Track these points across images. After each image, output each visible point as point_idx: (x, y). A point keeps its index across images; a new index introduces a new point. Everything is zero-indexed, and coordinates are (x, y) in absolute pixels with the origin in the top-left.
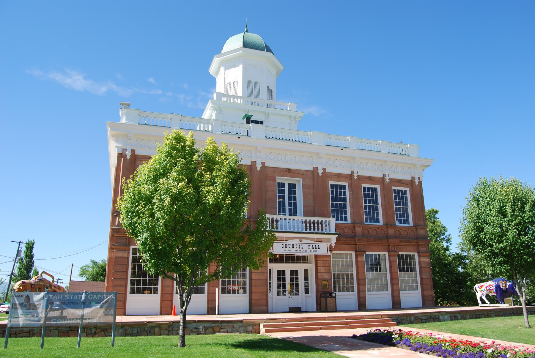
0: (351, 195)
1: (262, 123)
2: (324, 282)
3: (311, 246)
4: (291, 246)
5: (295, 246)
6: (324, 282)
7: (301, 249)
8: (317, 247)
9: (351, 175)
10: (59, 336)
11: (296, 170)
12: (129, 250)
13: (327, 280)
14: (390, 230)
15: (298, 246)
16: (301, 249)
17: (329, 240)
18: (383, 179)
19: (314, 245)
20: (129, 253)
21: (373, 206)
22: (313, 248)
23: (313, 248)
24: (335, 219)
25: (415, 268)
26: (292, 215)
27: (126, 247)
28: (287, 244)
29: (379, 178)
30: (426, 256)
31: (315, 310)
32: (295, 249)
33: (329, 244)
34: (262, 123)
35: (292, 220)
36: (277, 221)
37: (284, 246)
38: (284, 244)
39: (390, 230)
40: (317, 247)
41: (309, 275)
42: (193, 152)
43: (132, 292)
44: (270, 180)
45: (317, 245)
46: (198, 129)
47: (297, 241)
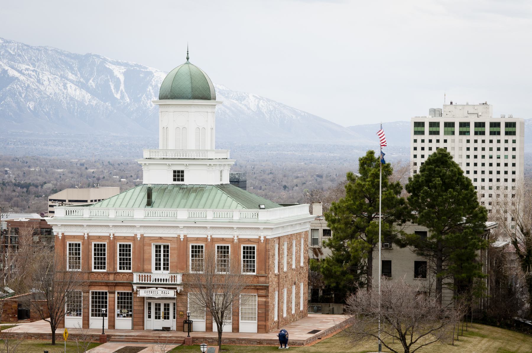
2: (181, 313)
17: (176, 288)
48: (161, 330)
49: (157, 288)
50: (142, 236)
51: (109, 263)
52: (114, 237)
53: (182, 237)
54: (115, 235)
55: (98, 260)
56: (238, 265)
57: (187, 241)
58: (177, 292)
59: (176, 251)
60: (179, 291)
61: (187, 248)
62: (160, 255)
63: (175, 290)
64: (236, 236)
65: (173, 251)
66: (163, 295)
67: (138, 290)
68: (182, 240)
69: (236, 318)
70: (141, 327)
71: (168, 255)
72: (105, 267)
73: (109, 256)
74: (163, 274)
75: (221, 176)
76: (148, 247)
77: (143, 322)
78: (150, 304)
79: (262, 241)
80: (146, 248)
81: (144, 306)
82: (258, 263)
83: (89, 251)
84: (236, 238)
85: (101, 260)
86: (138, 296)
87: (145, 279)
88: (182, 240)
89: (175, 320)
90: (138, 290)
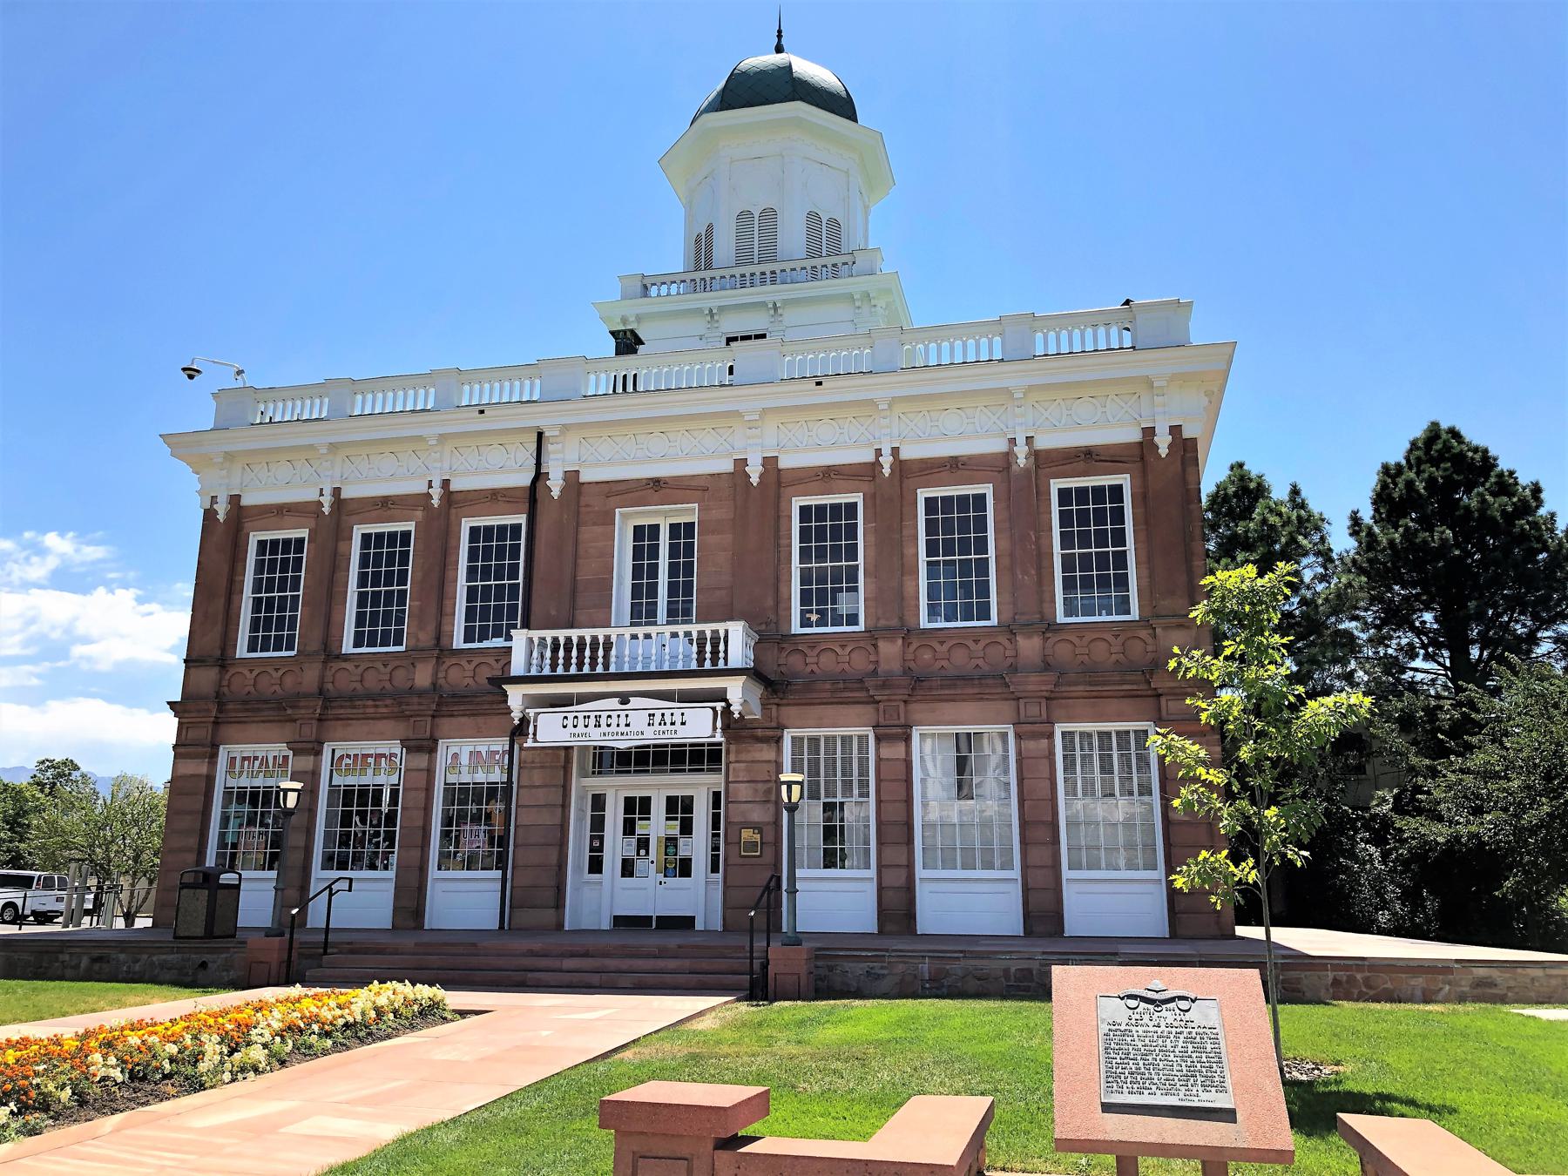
0: (1044, 557)
1: (763, 336)
2: (747, 834)
4: (592, 721)
5: (603, 721)
6: (747, 834)
7: (623, 728)
9: (873, 464)
11: (970, 457)
12: (1051, 736)
13: (757, 827)
14: (1022, 642)
16: (623, 728)
18: (1008, 457)
19: (667, 713)
20: (779, 751)
21: (487, 589)
22: (663, 722)
23: (663, 722)
24: (513, 632)
26: (639, 624)
27: (1045, 728)
28: (581, 715)
29: (1127, 446)
32: (604, 728)
34: (763, 336)
35: (641, 636)
36: (608, 645)
37: (570, 722)
38: (658, 714)
39: (1022, 642)
41: (589, 813)
43: (445, 860)
44: (595, 524)
45: (677, 713)
46: (1040, 351)
47: (614, 703)
49: (624, 698)
50: (770, 463)
51: (419, 616)
52: (448, 495)
53: (755, 472)
54: (454, 487)
55: (376, 604)
56: (1040, 583)
57: (779, 484)
58: (727, 711)
59: (728, 538)
60: (736, 708)
62: (653, 570)
63: (719, 706)
65: (713, 539)
66: (651, 735)
67: (531, 712)
68: (755, 480)
69: (896, 855)
70: (549, 915)
71: (689, 568)
72: (399, 633)
73: (419, 585)
74: (667, 642)
76: (598, 529)
77: (560, 889)
78: (598, 802)
79: (1163, 452)
80: (587, 533)
81: (565, 806)
82: (1146, 561)
83: (337, 564)
85: (376, 575)
86: (529, 743)
88: (755, 480)
89: (720, 875)
90: (531, 712)
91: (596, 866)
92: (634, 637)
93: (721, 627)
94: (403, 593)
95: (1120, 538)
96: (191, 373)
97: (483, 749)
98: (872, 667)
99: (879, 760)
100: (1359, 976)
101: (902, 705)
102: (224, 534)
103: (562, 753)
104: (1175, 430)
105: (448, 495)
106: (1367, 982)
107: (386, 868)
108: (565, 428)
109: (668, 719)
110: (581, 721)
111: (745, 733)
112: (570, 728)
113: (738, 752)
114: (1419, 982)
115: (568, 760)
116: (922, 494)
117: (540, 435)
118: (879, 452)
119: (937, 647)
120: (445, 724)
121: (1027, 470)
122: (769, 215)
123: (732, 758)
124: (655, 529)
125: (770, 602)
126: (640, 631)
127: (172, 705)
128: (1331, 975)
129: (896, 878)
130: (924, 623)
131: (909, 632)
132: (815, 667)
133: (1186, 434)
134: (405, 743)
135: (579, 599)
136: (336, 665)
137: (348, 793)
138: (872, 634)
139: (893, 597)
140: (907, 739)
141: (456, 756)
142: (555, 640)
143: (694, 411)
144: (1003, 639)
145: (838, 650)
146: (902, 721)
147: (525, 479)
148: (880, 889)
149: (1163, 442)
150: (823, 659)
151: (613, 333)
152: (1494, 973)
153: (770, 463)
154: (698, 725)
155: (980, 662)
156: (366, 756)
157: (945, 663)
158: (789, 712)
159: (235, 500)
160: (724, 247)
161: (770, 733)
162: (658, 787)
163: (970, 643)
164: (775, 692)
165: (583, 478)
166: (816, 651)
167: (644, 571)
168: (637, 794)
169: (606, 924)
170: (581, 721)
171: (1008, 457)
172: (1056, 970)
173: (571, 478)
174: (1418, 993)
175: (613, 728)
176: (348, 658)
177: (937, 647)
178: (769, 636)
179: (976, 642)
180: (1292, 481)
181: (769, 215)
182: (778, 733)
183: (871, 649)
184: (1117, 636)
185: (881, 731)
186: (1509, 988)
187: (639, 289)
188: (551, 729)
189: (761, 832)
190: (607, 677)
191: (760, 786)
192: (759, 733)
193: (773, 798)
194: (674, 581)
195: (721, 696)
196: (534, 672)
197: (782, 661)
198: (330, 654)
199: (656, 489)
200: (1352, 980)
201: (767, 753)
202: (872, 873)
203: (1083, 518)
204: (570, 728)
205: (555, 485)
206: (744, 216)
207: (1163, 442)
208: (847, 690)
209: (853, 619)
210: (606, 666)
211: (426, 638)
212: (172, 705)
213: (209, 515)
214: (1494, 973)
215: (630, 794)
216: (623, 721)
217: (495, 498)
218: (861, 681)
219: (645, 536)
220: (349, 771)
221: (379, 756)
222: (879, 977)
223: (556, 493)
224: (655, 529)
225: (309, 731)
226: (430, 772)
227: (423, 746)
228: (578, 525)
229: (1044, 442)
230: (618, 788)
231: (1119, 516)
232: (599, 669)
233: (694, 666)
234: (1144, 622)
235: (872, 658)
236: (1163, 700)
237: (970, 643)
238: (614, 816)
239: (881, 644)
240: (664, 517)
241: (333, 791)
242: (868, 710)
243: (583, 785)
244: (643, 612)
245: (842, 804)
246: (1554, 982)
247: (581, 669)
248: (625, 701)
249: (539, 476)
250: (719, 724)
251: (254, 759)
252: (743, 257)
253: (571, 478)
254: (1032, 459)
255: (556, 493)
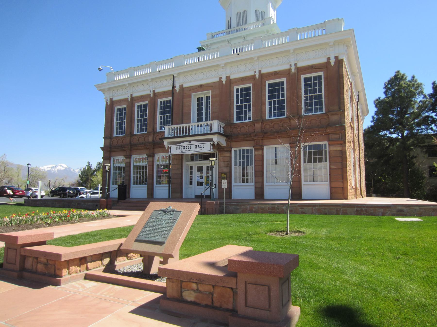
0: (299, 97)
3: (198, 146)
4: (183, 148)
5: (185, 148)
7: (190, 149)
8: (202, 146)
10: (347, 180)
13: (225, 173)
15: (188, 148)
17: (211, 140)
18: (290, 70)
19: (200, 145)
22: (199, 147)
25: (134, 169)
30: (338, 144)
31: (167, 196)
33: (212, 142)
37: (178, 148)
38: (198, 145)
40: (202, 146)
42: (416, 81)
45: (202, 145)
47: (187, 143)
48: (42, 203)
49: (190, 141)
50: (228, 78)
52: (155, 94)
58: (214, 144)
60: (216, 143)
61: (230, 92)
62: (202, 109)
63: (212, 142)
64: (293, 65)
67: (170, 146)
68: (224, 82)
75: (276, 156)
78: (191, 168)
80: (185, 100)
81: (182, 169)
84: (293, 68)
87: (177, 131)
91: (191, 183)
92: (198, 126)
93: (212, 122)
94: (146, 119)
95: (320, 90)
96: (100, 70)
97: (165, 156)
98: (253, 131)
99: (255, 155)
100: (364, 209)
101: (261, 141)
102: (110, 107)
103: (181, 156)
104: (336, 58)
105: (155, 94)
106: (366, 211)
107: (145, 184)
108: (179, 74)
109: (200, 147)
110: (180, 148)
111: (222, 149)
112: (178, 150)
113: (221, 154)
114: (381, 210)
115: (182, 158)
116: (267, 83)
117: (173, 76)
118: (255, 72)
119: (270, 124)
120: (156, 150)
121: (295, 73)
122: (245, 12)
123: (219, 156)
124: (202, 98)
125: (228, 115)
126: (199, 124)
127: (101, 148)
128: (356, 209)
129: (259, 185)
130: (267, 118)
131: (263, 120)
132: (239, 132)
133: (340, 58)
134: (147, 155)
135: (184, 117)
136: (133, 137)
137: (137, 167)
138: (254, 122)
139: (260, 112)
140: (262, 149)
141: (159, 158)
142: (180, 127)
143: (210, 65)
144: (288, 121)
145: (245, 127)
146: (261, 144)
147: (170, 88)
148: (255, 188)
149: (332, 61)
150: (242, 129)
151: (197, 48)
152: (404, 208)
153: (228, 78)
154: (207, 148)
155: (282, 128)
156: (140, 158)
157: (272, 128)
158: (233, 144)
159: (111, 99)
160: (234, 23)
161: (228, 149)
162: (205, 164)
163: (279, 123)
164: (229, 139)
165: (184, 86)
166: (240, 127)
167: (200, 109)
168: (200, 166)
169: (193, 197)
170: (180, 148)
171: (290, 70)
172: (24, 203)
173: (181, 86)
174: (381, 213)
175: (188, 149)
176: (135, 135)
177: (270, 124)
178: (228, 124)
179: (281, 122)
180: (433, 80)
181: (245, 12)
182: (230, 149)
183: (253, 126)
184: (318, 118)
185: (255, 147)
186: (408, 212)
187: (211, 36)
188: (174, 150)
189: (226, 174)
190: (186, 136)
191: (226, 163)
192: (225, 149)
193: (229, 165)
194: (206, 111)
195: (211, 140)
196: (170, 136)
197: (231, 131)
198: (131, 134)
199: (201, 87)
200: (362, 210)
201: (227, 154)
202: (254, 184)
203: (310, 86)
204: (178, 150)
205: (177, 89)
206: (239, 14)
207: (332, 61)
208: (247, 137)
209: (250, 119)
210: (189, 133)
211: (151, 130)
212: (101, 148)
213: (107, 103)
214: (404, 208)
215: (198, 166)
216: (190, 147)
217: (165, 94)
218: (250, 135)
219: (200, 100)
220: (137, 162)
221: (143, 158)
222: (237, 209)
223: (177, 91)
224: (202, 98)
225: (128, 153)
226: (153, 162)
227: (151, 155)
228: (183, 99)
229: (300, 65)
230: (196, 164)
231: (320, 84)
232: (187, 134)
233: (209, 132)
234: (326, 113)
235: (254, 128)
236: (330, 135)
237: (279, 123)
238: (195, 170)
239: (256, 124)
240: (204, 94)
241: (134, 167)
242: (252, 142)
243: (186, 164)
244: (199, 119)
245: (247, 167)
246: (422, 210)
247: (186, 134)
248: (190, 142)
249: (174, 87)
250: (212, 147)
251: (119, 160)
252: (238, 24)
253: (181, 86)
254: (296, 70)
255: (177, 91)
